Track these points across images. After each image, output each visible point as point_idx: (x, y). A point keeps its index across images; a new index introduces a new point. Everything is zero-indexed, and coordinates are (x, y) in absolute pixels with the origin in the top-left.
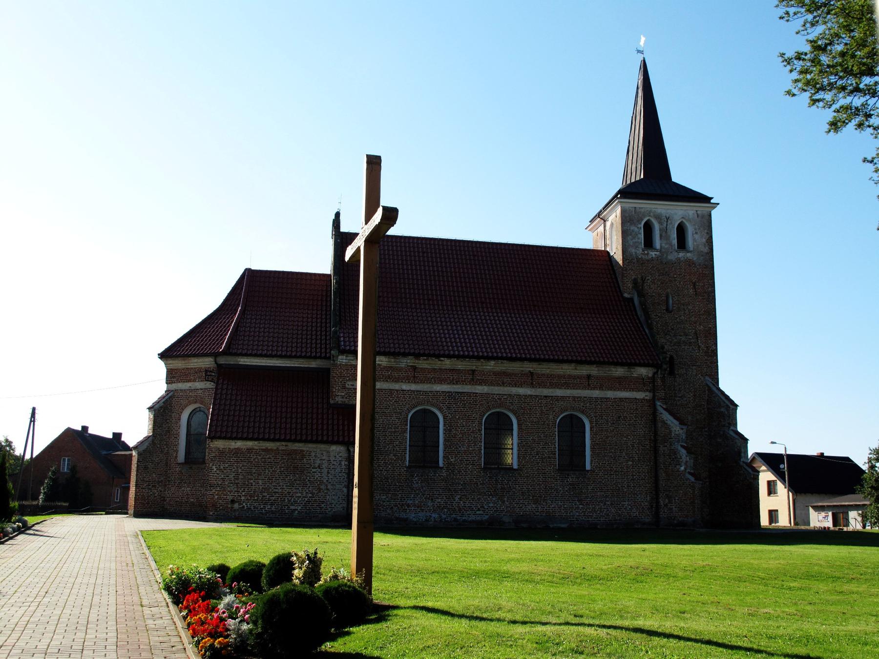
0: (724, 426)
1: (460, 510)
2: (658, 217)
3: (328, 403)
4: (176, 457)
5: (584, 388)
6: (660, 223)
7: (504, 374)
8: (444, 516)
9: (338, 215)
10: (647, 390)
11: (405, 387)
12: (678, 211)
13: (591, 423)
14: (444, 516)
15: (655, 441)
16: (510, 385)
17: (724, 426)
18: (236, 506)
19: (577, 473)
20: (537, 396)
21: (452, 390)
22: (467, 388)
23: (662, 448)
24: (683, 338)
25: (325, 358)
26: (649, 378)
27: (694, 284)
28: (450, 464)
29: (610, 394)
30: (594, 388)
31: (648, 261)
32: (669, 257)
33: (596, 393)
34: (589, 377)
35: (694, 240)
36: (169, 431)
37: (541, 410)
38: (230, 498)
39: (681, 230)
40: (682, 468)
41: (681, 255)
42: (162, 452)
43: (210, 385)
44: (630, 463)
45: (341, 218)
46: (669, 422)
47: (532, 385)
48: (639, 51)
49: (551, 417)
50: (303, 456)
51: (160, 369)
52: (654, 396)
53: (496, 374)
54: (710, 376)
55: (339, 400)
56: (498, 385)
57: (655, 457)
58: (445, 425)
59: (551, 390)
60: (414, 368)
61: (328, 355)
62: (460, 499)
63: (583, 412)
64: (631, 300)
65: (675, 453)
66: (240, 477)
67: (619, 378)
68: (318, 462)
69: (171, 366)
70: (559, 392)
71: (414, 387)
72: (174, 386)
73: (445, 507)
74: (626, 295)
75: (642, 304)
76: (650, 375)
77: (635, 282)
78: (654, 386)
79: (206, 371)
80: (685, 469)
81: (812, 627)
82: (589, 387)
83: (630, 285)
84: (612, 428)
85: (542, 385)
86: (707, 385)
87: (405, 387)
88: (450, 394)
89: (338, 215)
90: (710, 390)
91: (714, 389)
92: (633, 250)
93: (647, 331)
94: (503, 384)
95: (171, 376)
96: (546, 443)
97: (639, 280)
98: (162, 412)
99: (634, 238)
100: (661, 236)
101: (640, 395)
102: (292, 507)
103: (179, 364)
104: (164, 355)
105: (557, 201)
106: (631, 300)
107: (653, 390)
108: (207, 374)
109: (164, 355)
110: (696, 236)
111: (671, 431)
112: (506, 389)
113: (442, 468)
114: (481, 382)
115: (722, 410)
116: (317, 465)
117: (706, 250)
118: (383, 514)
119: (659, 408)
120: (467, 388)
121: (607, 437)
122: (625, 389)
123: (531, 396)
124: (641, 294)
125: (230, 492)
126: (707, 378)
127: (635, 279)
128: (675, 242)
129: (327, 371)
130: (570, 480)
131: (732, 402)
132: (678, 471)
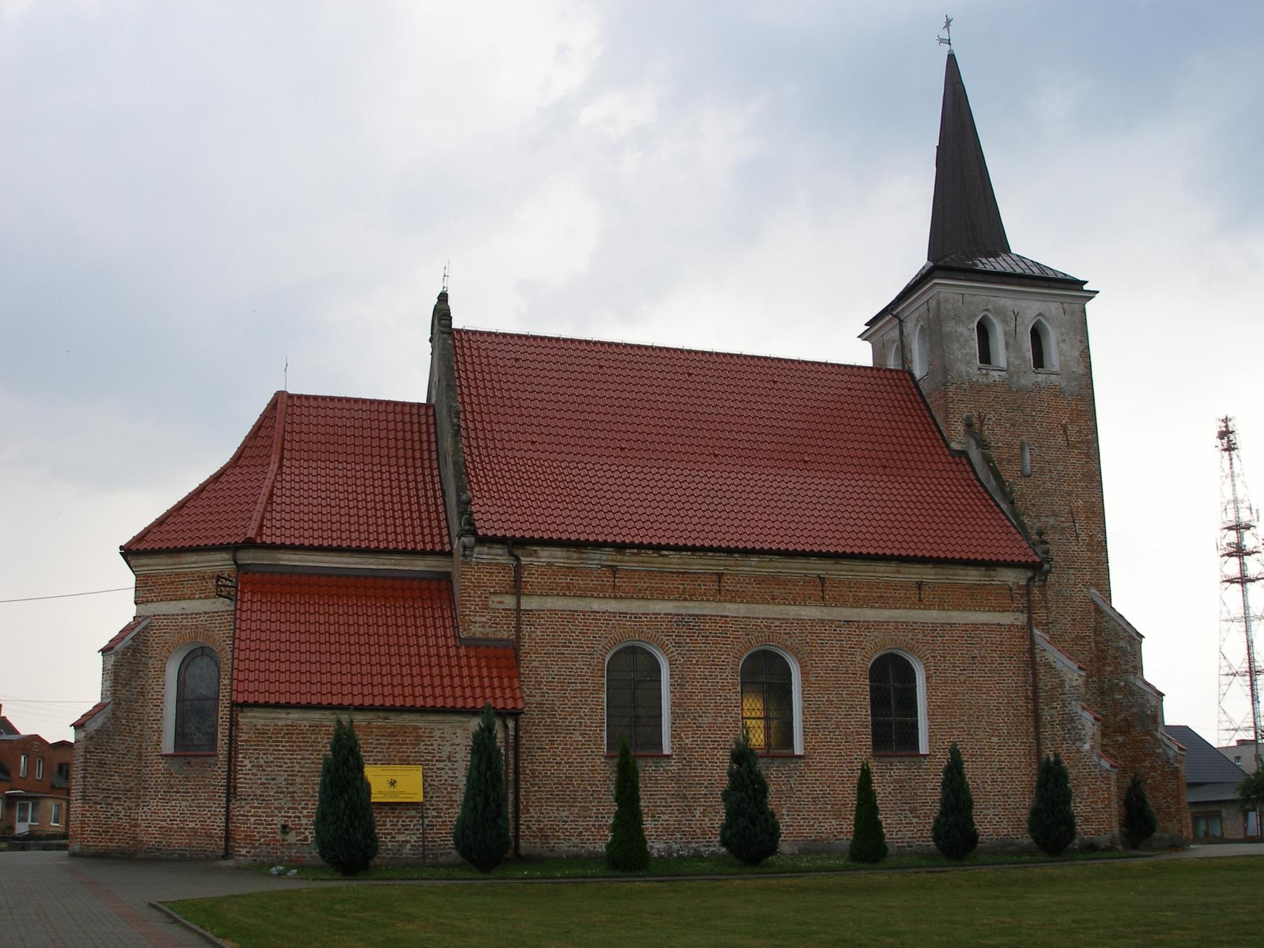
0: (1126, 672)
1: (704, 834)
2: (1000, 312)
3: (457, 637)
4: (158, 743)
5: (912, 607)
6: (1005, 322)
7: (775, 580)
8: (676, 847)
9: (443, 297)
10: (1018, 610)
11: (596, 605)
12: (1031, 307)
13: (927, 669)
14: (676, 847)
15: (1035, 698)
16: (785, 601)
17: (1126, 672)
18: (292, 838)
19: (907, 760)
20: (832, 621)
21: (683, 612)
22: (709, 608)
23: (1046, 714)
24: (1052, 521)
25: (442, 553)
26: (1020, 587)
27: (1064, 428)
28: (682, 748)
29: (957, 617)
30: (929, 607)
31: (988, 386)
32: (1022, 381)
33: (934, 615)
34: (920, 585)
35: (1061, 353)
36: (142, 694)
37: (842, 646)
38: (279, 821)
39: (1037, 335)
40: (1087, 747)
41: (1040, 378)
42: (130, 732)
43: (222, 605)
44: (995, 739)
45: (451, 303)
46: (1059, 666)
47: (823, 601)
48: (942, 41)
49: (859, 658)
50: (419, 739)
51: (126, 578)
52: (1030, 620)
53: (759, 580)
54: (1097, 586)
55: (477, 631)
56: (764, 601)
57: (1037, 727)
58: (672, 676)
59: (856, 611)
60: (614, 570)
61: (447, 548)
62: (704, 813)
63: (796, 654)
64: (963, 454)
65: (1072, 720)
66: (298, 780)
67: (970, 587)
68: (447, 749)
69: (144, 570)
70: (870, 614)
71: (613, 606)
72: (152, 608)
73: (678, 830)
74: (954, 446)
75: (987, 460)
76: (1023, 582)
77: (969, 425)
78: (1029, 601)
79: (219, 578)
80: (1092, 747)
81: (343, 884)
82: (920, 603)
83: (961, 428)
84: (962, 678)
85: (841, 601)
86: (1093, 602)
87: (596, 605)
88: (680, 619)
89: (443, 297)
90: (1098, 610)
91: (1106, 608)
92: (963, 368)
93: (1004, 506)
94: (773, 600)
95: (145, 590)
96: (852, 707)
97: (975, 421)
98: (127, 658)
99: (964, 346)
100: (1007, 344)
101: (1006, 618)
102: (401, 838)
103: (159, 565)
104: (129, 552)
105: (810, 288)
106: (963, 454)
107: (1029, 609)
108: (220, 586)
109: (129, 552)
110: (1065, 347)
111: (1063, 682)
112: (778, 608)
113: (668, 757)
114: (734, 597)
115: (1122, 644)
116: (444, 755)
117: (1080, 370)
118: (564, 846)
119: (1038, 640)
120: (709, 608)
121: (955, 695)
122: (978, 607)
123: (822, 621)
124: (982, 444)
125: (280, 809)
126: (1093, 590)
127: (968, 418)
128: (1030, 355)
129: (446, 578)
130: (895, 773)
131: (1138, 634)
132: (1078, 751)
